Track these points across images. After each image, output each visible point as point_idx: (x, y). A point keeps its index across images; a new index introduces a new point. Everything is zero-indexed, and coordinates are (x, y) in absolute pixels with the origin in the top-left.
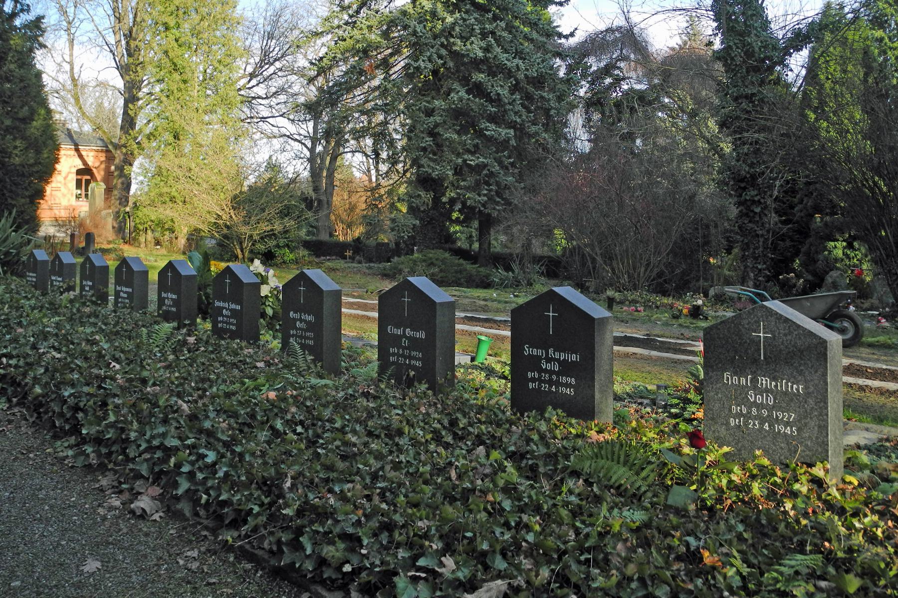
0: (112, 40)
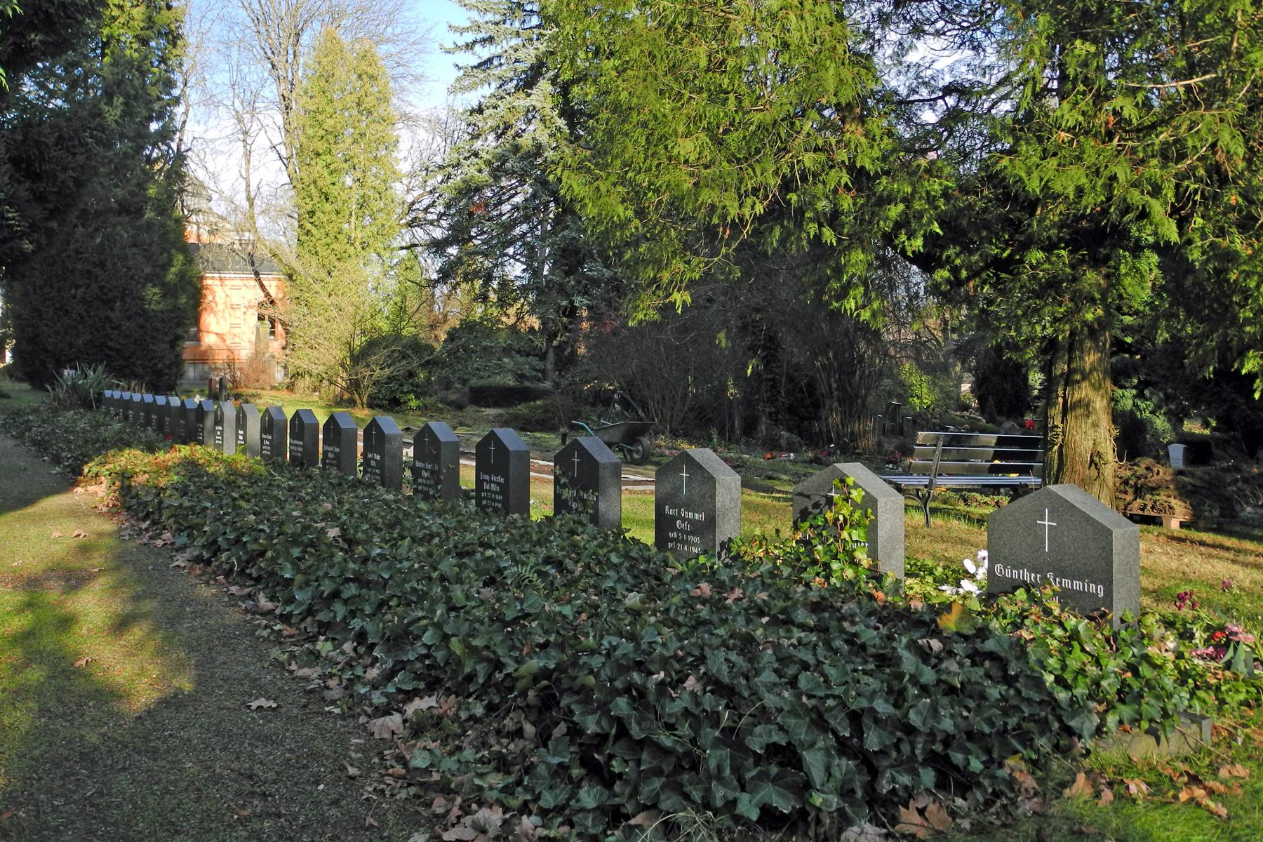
0: (284, 153)
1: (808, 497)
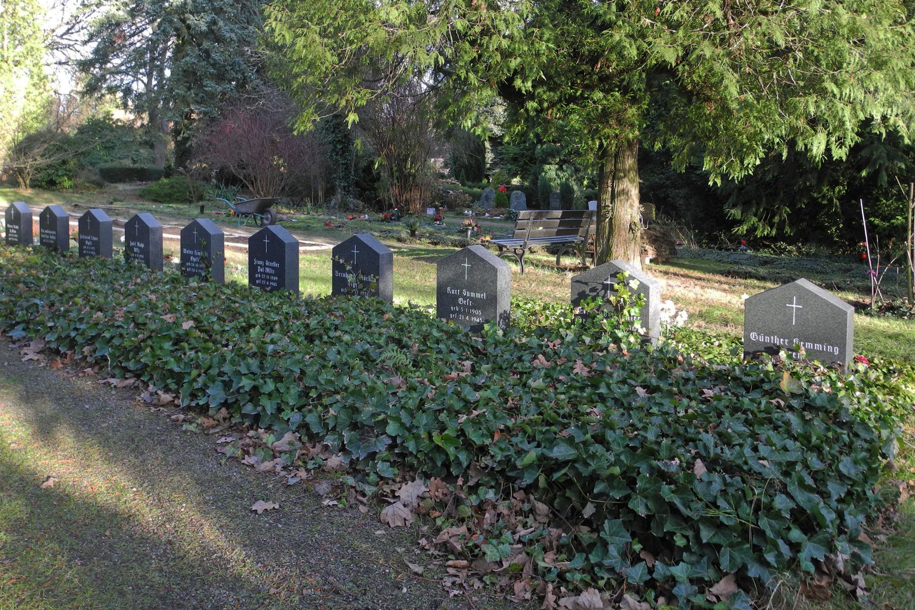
1: (586, 283)
